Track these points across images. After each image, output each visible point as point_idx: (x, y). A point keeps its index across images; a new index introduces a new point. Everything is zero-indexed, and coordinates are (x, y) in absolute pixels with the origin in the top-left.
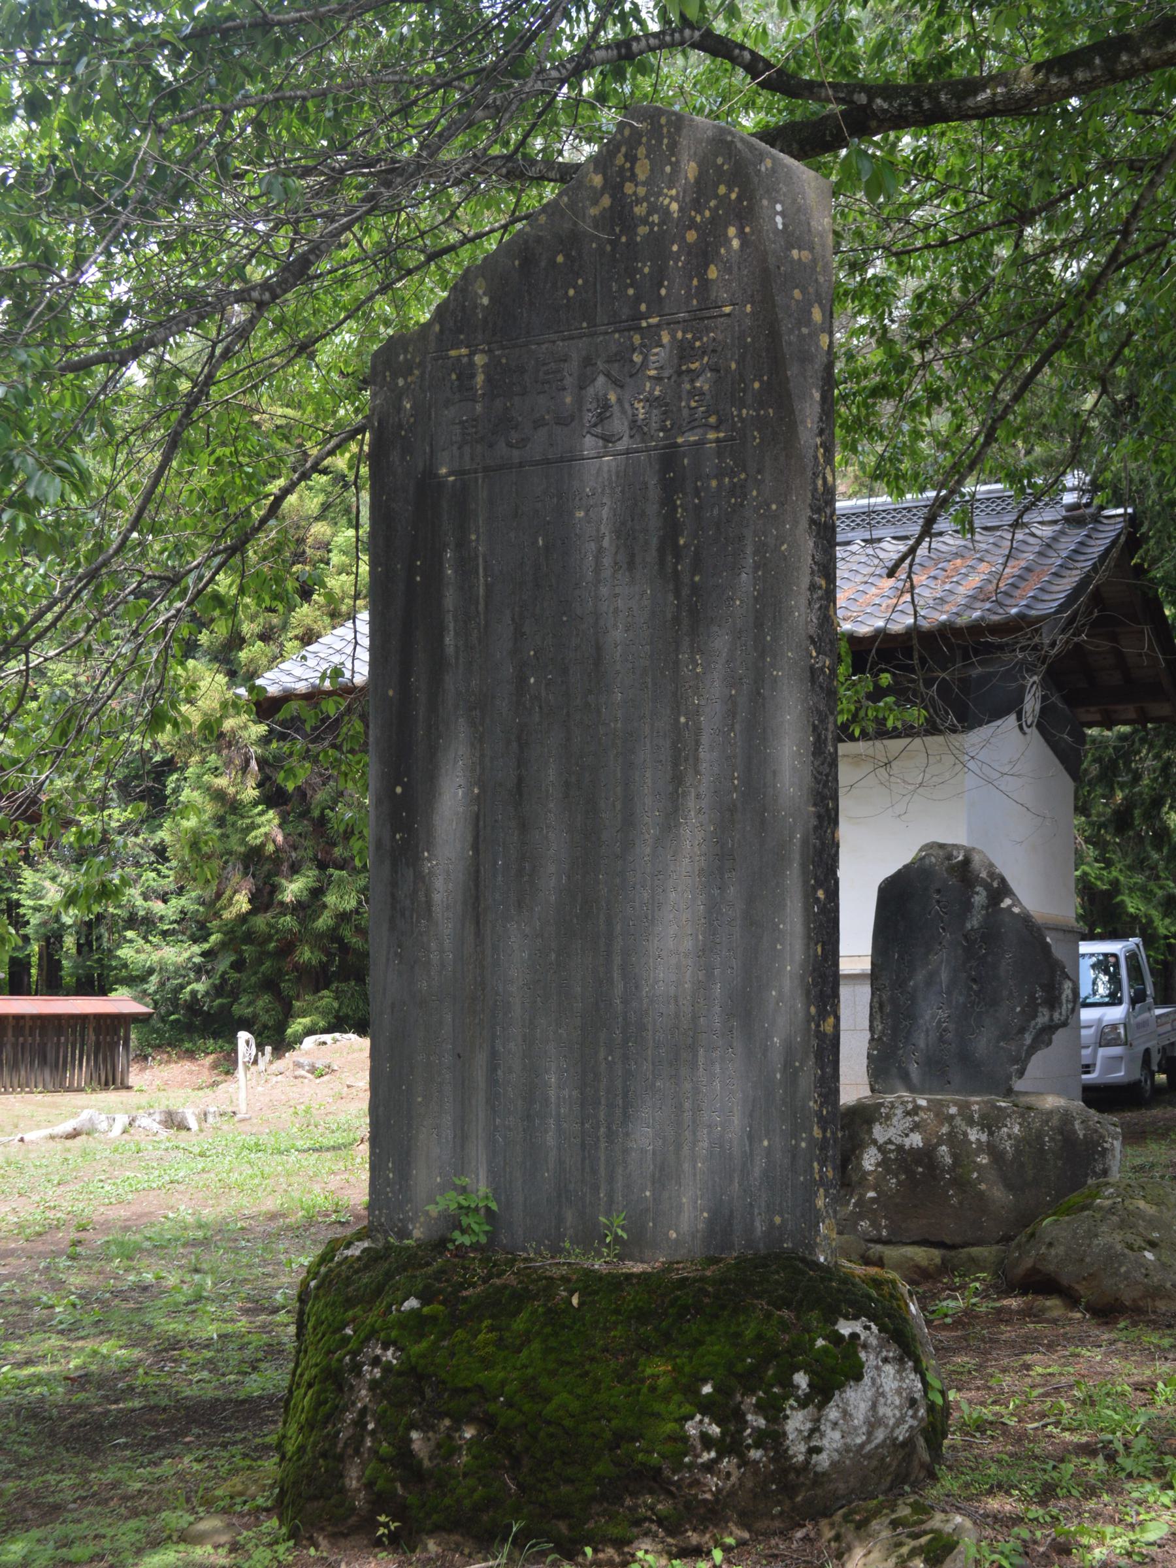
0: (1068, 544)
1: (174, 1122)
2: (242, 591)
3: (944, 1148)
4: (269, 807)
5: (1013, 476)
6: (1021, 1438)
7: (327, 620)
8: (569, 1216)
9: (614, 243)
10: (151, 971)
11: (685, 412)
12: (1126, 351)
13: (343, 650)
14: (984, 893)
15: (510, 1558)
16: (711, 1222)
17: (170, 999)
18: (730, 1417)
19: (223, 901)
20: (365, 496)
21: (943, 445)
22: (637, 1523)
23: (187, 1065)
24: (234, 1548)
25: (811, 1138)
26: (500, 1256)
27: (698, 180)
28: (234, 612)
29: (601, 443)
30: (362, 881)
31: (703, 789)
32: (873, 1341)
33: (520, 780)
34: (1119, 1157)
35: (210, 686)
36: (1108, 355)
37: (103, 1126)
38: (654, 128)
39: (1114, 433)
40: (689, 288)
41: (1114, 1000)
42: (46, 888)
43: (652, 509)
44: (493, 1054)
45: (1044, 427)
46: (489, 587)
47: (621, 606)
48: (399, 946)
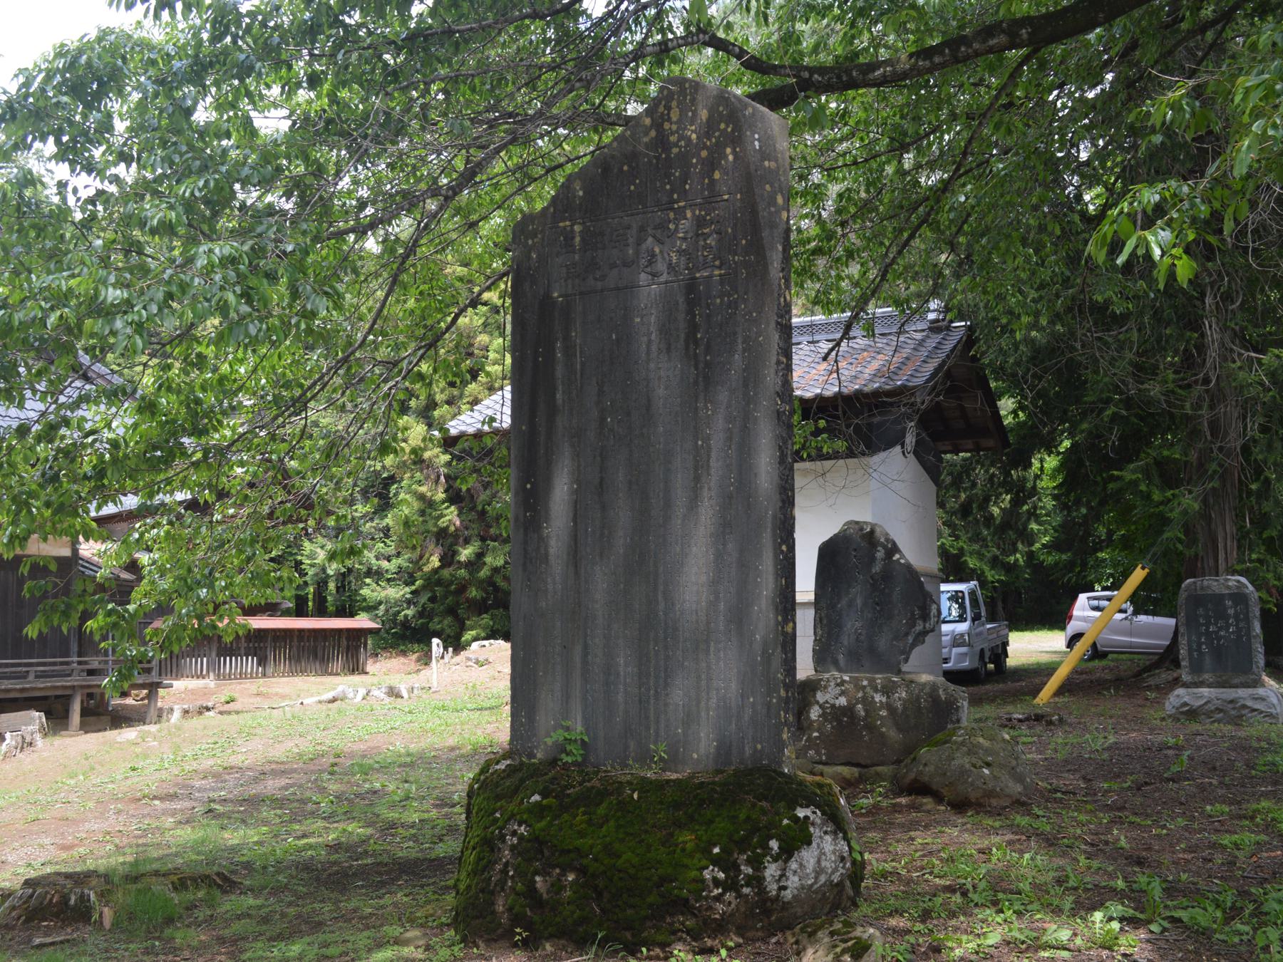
0: (931, 343)
1: (393, 693)
2: (435, 371)
4: (452, 504)
5: (897, 303)
6: (909, 881)
7: (487, 392)
8: (632, 744)
9: (658, 158)
10: (380, 603)
11: (701, 258)
12: (965, 227)
13: (494, 409)
15: (596, 955)
16: (718, 748)
17: (391, 620)
18: (729, 866)
19: (424, 560)
20: (509, 318)
21: (856, 284)
22: (674, 933)
23: (402, 660)
24: (428, 948)
25: (779, 697)
26: (590, 769)
27: (708, 120)
28: (430, 384)
30: (507, 548)
31: (712, 484)
32: (819, 821)
33: (602, 479)
34: (967, 713)
35: (416, 431)
36: (954, 229)
37: (351, 695)
38: (684, 90)
39: (957, 276)
40: (703, 184)
41: (961, 619)
42: (316, 552)
43: (681, 316)
44: (586, 647)
45: (917, 273)
46: (583, 364)
47: (663, 374)
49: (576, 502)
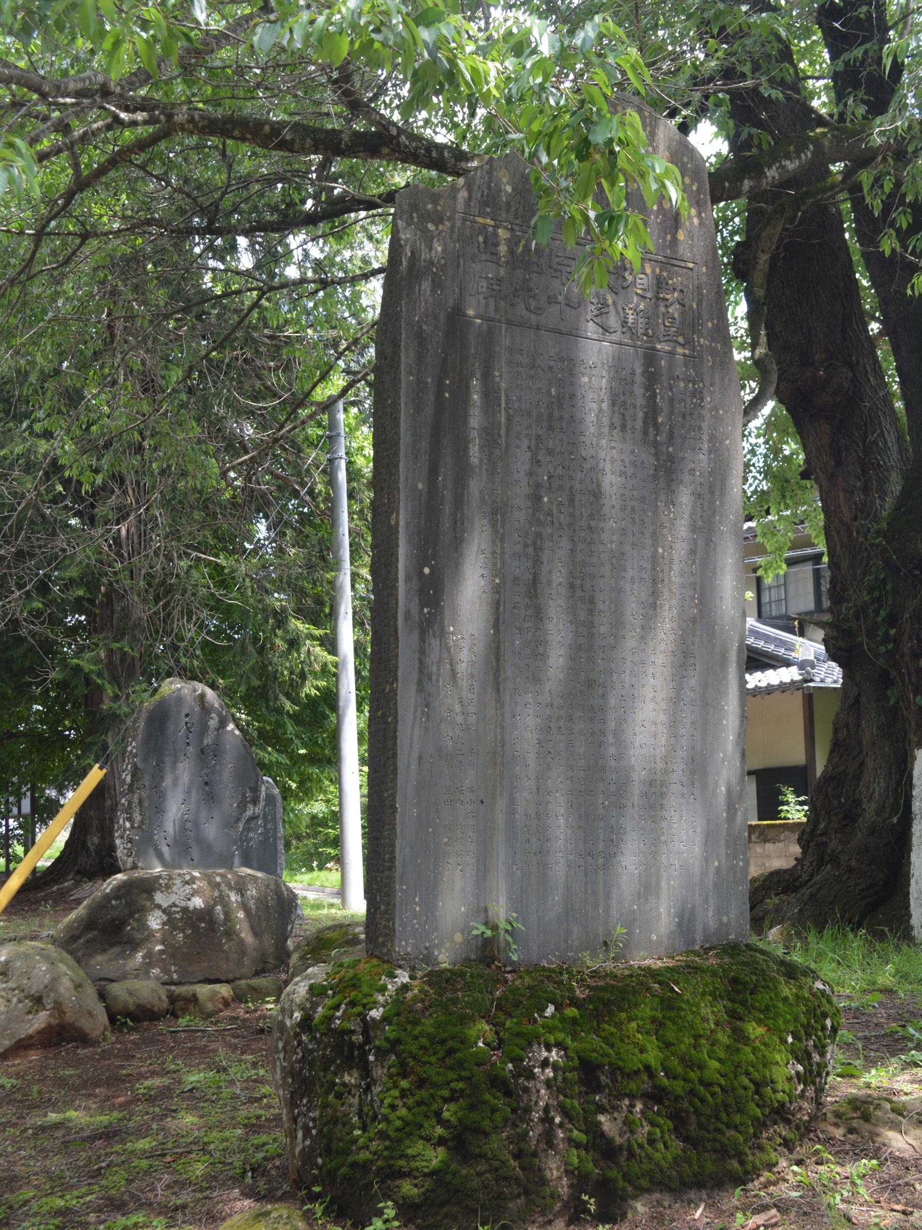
3: (219, 907)
8: (576, 931)
14: (217, 719)
29: (600, 330)
43: (639, 390)
46: (509, 419)
48: (427, 706)
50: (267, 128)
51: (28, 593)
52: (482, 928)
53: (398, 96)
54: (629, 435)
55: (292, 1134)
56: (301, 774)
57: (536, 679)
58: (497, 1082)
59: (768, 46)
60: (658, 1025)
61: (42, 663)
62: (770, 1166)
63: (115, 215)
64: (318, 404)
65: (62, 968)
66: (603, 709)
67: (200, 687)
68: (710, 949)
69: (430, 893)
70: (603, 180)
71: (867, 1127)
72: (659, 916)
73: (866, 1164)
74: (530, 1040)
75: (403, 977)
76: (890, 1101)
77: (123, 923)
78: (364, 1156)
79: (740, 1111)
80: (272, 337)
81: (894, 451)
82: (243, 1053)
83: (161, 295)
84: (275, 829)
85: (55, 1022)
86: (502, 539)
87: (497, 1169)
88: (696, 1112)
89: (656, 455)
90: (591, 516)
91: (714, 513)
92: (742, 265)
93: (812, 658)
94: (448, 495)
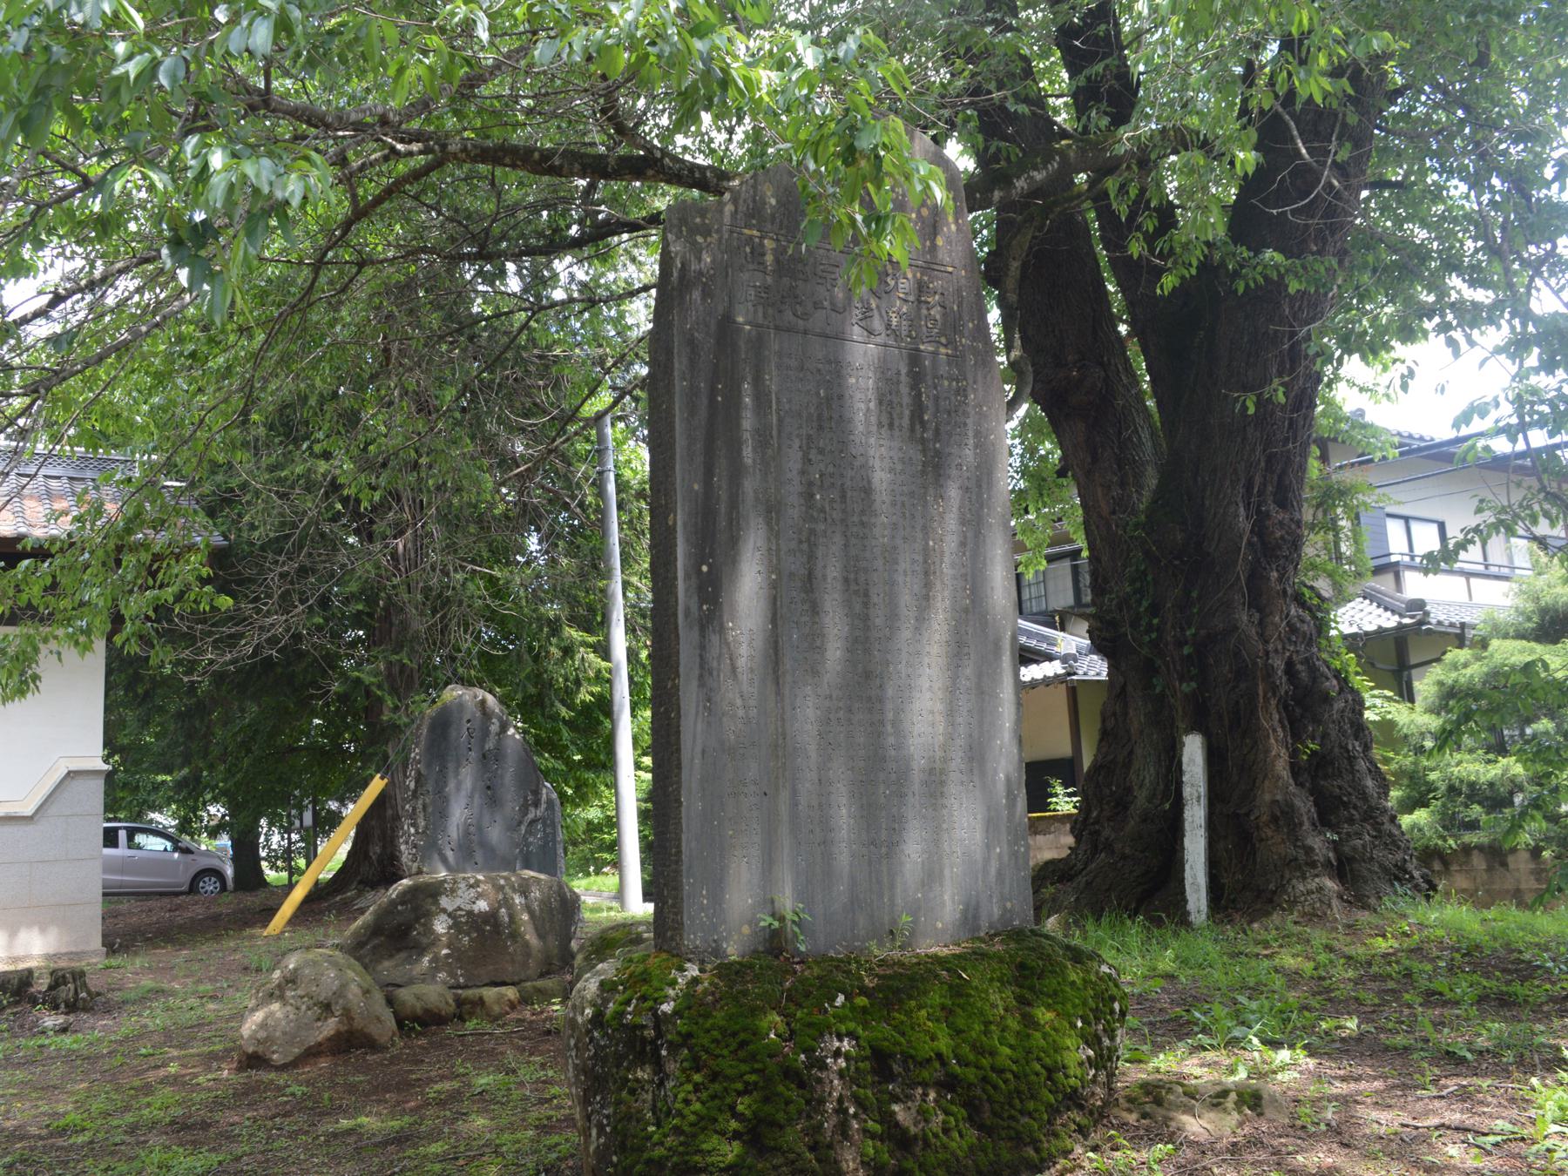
8: (862, 921)
16: (965, 912)
43: (904, 390)
46: (780, 420)
47: (880, 457)
49: (775, 598)
50: (536, 155)
51: (310, 607)
52: (770, 920)
53: (657, 125)
54: (897, 433)
55: (586, 1133)
56: (576, 779)
57: (815, 672)
58: (790, 1074)
59: (1012, 65)
60: (948, 1012)
61: (324, 674)
62: (1066, 1153)
63: (389, 245)
64: (587, 420)
65: (351, 974)
66: (881, 700)
67: (481, 693)
68: (995, 935)
69: (717, 885)
70: (869, 185)
71: (1161, 1111)
72: (943, 904)
73: (1161, 1149)
74: (821, 1030)
75: (693, 971)
76: (1182, 1085)
77: (410, 927)
78: (659, 1152)
79: (1033, 1097)
80: (540, 357)
81: (1147, 447)
82: (531, 1055)
83: (434, 320)
84: (554, 834)
85: (344, 1028)
86: (777, 536)
87: (793, 1162)
88: (990, 1100)
89: (924, 451)
90: (863, 512)
91: (982, 507)
92: (993, 272)
93: (1074, 651)
94: (723, 495)
